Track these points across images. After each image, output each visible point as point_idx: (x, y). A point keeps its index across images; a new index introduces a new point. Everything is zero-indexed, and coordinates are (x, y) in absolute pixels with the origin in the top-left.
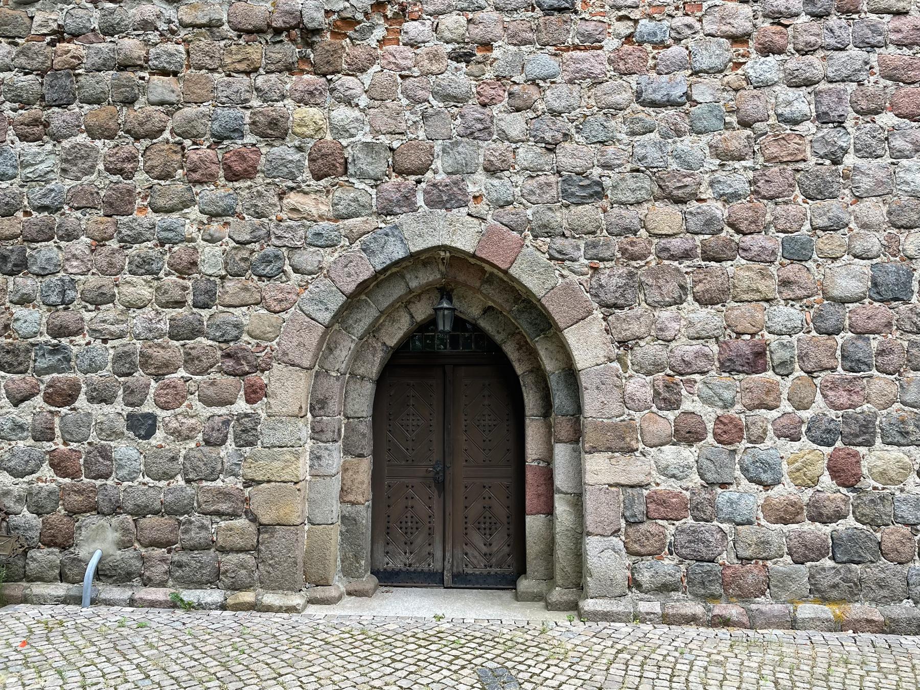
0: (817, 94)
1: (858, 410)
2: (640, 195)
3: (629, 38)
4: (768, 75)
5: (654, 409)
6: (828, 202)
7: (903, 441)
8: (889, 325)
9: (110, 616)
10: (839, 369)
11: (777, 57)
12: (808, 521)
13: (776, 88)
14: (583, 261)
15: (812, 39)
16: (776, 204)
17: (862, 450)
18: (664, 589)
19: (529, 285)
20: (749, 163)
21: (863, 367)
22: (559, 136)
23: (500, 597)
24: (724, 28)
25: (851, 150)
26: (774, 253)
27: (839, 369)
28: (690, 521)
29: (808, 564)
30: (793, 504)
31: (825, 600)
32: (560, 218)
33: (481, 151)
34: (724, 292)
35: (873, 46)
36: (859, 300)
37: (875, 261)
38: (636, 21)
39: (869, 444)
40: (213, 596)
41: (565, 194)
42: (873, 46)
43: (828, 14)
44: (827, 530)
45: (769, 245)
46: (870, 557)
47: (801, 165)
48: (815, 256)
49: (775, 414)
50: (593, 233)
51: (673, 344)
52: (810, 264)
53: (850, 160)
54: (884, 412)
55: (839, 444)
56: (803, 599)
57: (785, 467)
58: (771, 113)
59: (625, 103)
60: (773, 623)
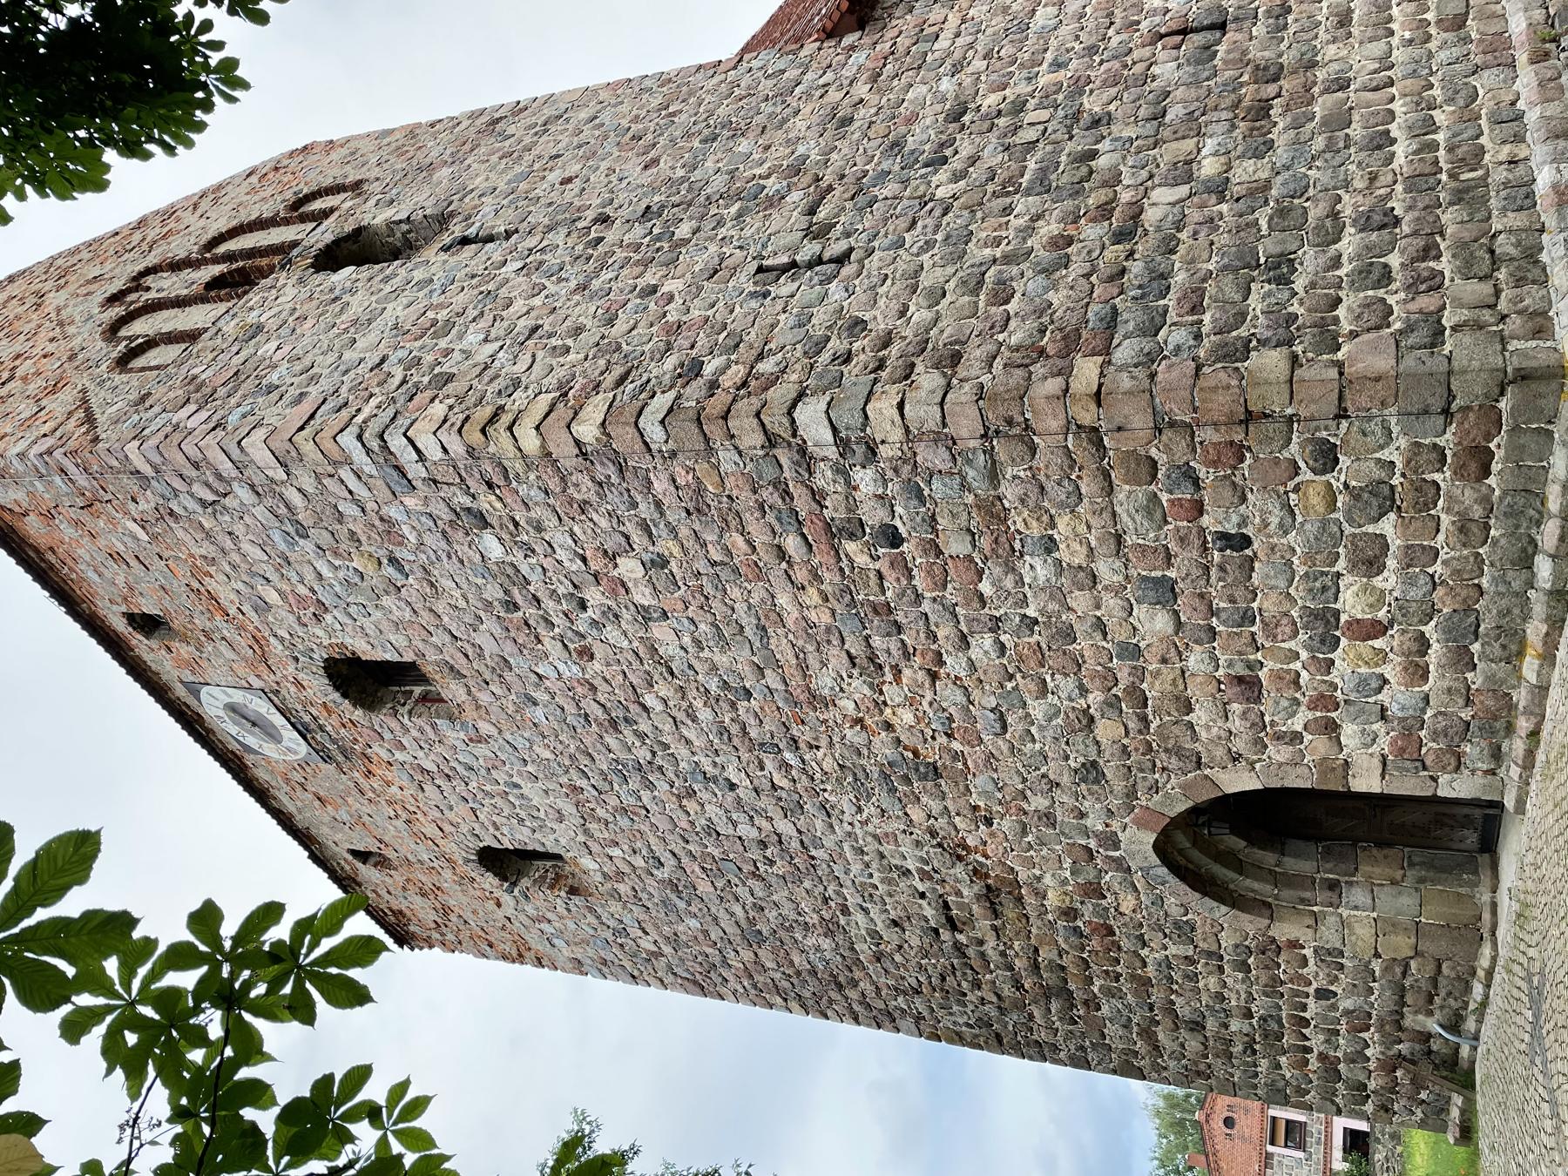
0: (972, 633)
1: (1298, 620)
2: (1089, 741)
3: (949, 736)
4: (964, 665)
5: (1302, 747)
6: (830, 345)
7: (1333, 590)
8: (1201, 596)
9: (1486, 1032)
10: (1252, 629)
11: (945, 656)
12: (1427, 658)
13: (973, 657)
14: (1157, 776)
15: (922, 635)
16: (1084, 662)
17: (1344, 618)
18: (1497, 755)
19: (1184, 808)
20: (1048, 679)
21: (1250, 613)
22: (1044, 781)
23: (1505, 838)
24: (927, 686)
25: (1022, 611)
26: (1135, 668)
27: (1252, 629)
28: (1423, 733)
29: (1476, 661)
30: (1406, 669)
31: (1521, 654)
32: (1119, 786)
33: (1066, 820)
34: (1178, 698)
35: (918, 595)
36: (1176, 613)
37: (1133, 601)
38: (934, 731)
39: (1337, 614)
40: (1478, 989)
41: (1096, 781)
42: (918, 595)
43: (896, 621)
44: (1435, 646)
45: (1126, 671)
46: (1472, 618)
47: (1044, 646)
48: (1134, 641)
49: (1304, 674)
50: (1129, 768)
51: (1234, 730)
52: (1142, 645)
53: (1031, 612)
54: (1299, 601)
55: (1338, 633)
56: (1517, 670)
57: (1363, 670)
58: (997, 662)
59: (1007, 744)
60: (1540, 702)
